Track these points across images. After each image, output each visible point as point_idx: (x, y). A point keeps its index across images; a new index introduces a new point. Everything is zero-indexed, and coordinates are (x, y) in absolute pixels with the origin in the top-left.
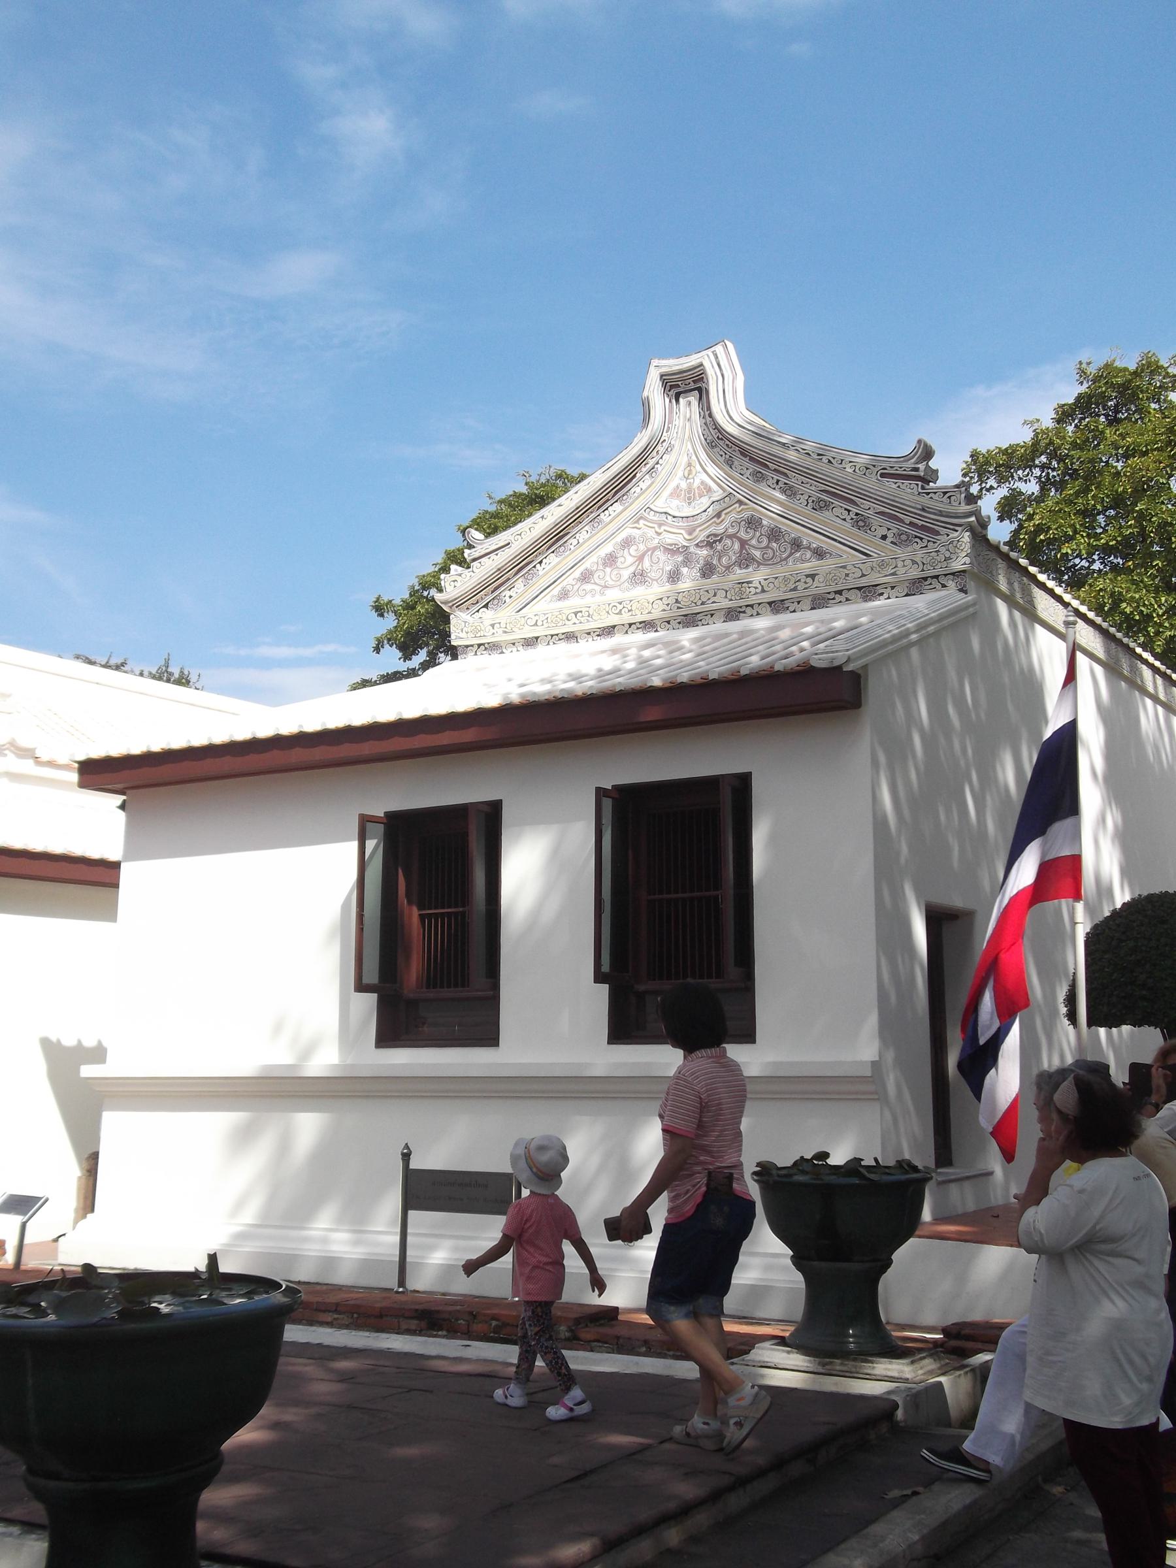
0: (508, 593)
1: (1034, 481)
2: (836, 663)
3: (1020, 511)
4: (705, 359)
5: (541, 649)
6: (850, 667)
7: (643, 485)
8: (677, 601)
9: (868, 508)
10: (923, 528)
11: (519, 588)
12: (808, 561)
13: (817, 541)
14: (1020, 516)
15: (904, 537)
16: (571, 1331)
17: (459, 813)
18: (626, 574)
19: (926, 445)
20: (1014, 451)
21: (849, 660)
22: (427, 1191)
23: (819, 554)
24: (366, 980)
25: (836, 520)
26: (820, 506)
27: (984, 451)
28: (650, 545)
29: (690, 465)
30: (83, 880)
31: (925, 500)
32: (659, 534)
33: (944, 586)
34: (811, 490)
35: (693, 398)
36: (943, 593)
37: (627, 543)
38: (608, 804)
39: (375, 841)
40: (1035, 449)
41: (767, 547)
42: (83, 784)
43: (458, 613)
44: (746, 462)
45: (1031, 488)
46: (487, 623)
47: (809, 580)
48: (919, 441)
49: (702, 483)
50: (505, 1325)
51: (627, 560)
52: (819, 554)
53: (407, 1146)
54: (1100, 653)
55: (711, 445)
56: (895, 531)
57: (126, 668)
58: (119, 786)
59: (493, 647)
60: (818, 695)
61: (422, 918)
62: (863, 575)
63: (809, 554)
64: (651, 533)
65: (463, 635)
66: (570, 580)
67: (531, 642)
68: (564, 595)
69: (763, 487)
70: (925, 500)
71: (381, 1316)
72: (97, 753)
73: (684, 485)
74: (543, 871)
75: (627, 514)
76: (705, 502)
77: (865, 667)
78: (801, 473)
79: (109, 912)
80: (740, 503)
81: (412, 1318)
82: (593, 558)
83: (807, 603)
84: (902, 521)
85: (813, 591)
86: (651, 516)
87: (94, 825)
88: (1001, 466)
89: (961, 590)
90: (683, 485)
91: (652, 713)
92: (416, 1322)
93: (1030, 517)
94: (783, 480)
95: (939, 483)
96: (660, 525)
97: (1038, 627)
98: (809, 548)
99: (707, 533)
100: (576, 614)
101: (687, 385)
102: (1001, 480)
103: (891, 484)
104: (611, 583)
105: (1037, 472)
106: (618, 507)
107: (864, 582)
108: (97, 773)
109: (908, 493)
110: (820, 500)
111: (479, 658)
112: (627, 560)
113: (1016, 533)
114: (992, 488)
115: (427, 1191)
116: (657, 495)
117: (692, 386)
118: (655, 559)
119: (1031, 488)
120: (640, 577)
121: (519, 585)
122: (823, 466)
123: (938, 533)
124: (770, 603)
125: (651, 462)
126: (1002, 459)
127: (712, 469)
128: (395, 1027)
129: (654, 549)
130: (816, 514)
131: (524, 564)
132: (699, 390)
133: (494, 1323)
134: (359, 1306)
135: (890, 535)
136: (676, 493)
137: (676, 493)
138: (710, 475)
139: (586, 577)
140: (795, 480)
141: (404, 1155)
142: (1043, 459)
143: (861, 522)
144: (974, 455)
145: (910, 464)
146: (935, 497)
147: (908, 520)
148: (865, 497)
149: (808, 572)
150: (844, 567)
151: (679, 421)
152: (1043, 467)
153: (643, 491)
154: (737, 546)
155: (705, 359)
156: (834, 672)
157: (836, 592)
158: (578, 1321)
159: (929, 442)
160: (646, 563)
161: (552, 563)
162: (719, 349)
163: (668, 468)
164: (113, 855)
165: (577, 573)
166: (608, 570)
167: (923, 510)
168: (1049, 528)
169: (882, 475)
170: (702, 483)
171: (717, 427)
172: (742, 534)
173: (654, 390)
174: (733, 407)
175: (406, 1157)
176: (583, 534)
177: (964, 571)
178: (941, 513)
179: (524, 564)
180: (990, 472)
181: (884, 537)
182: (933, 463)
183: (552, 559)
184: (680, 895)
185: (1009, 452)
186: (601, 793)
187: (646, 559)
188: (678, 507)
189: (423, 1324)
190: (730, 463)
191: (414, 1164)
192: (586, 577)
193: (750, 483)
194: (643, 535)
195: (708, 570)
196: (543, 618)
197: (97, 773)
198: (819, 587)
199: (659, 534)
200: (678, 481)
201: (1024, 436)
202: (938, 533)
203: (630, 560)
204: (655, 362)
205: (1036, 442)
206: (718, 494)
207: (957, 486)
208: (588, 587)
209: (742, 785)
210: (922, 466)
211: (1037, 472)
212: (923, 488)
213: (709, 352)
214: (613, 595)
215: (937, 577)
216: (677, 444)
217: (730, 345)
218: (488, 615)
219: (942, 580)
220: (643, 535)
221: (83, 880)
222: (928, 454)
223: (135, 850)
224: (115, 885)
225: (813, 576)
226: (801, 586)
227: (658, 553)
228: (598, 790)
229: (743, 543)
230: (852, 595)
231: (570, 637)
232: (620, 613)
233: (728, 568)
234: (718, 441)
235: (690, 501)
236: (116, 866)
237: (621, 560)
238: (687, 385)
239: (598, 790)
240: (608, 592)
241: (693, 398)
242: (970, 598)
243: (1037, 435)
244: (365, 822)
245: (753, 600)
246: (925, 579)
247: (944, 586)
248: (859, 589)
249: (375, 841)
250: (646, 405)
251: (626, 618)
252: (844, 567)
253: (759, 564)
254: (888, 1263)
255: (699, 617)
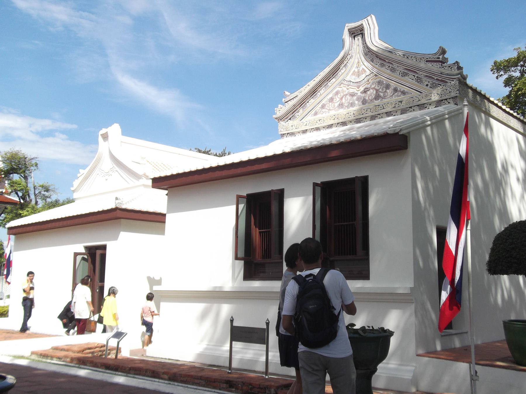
0: (297, 114)
1: (518, 72)
2: (396, 131)
3: (513, 83)
4: (364, 22)
5: (308, 134)
6: (401, 133)
7: (342, 71)
8: (354, 114)
9: (422, 74)
10: (441, 81)
11: (301, 112)
12: (400, 96)
13: (406, 89)
14: (513, 85)
15: (434, 85)
16: (276, 391)
17: (267, 194)
18: (337, 105)
19: (443, 48)
20: (510, 61)
21: (401, 130)
22: (239, 334)
23: (404, 93)
24: (239, 256)
25: (409, 80)
26: (404, 75)
27: (499, 61)
28: (345, 94)
29: (358, 62)
30: (154, 220)
31: (442, 70)
32: (348, 89)
33: (449, 103)
34: (401, 69)
35: (360, 37)
36: (449, 105)
37: (337, 93)
38: (318, 189)
39: (243, 205)
40: (518, 59)
41: (385, 92)
42: (153, 187)
43: (281, 122)
44: (378, 60)
45: (517, 74)
46: (290, 125)
47: (400, 103)
48: (440, 47)
49: (363, 69)
50: (254, 387)
51: (337, 99)
52: (404, 93)
53: (268, 320)
54: (522, 130)
55: (366, 54)
56: (431, 82)
57: (210, 153)
58: (166, 187)
59: (292, 134)
60: (389, 145)
61: (260, 232)
62: (419, 100)
63: (400, 93)
64: (345, 89)
65: (282, 130)
66: (318, 108)
67: (305, 132)
68: (316, 114)
69: (383, 69)
70: (442, 70)
71: (214, 382)
72: (157, 176)
73: (356, 70)
74: (298, 215)
75: (337, 82)
76: (364, 76)
77: (409, 133)
78: (397, 63)
79: (162, 231)
80: (376, 75)
81: (224, 383)
82: (326, 100)
83: (399, 112)
84: (433, 78)
85: (401, 107)
86: (345, 83)
87: (157, 201)
88: (505, 66)
89: (455, 104)
90: (358, 71)
91: (334, 154)
92: (225, 385)
93: (516, 85)
94: (391, 66)
95: (448, 63)
96: (348, 86)
97: (492, 121)
98: (400, 91)
99: (364, 87)
100: (319, 120)
101: (357, 32)
102: (505, 73)
103: (429, 65)
104: (332, 108)
105: (519, 68)
106: (334, 80)
107: (419, 103)
108: (159, 182)
109: (435, 68)
110: (404, 72)
111: (288, 138)
112: (337, 99)
113: (511, 91)
114: (502, 75)
115: (239, 334)
116: (347, 74)
117: (360, 33)
118: (346, 99)
119: (517, 74)
120: (341, 106)
121: (301, 111)
122: (405, 60)
123: (447, 82)
124: (386, 113)
125: (345, 62)
126: (506, 64)
127: (366, 63)
128: (249, 275)
129: (346, 95)
130: (403, 78)
131: (302, 103)
132: (362, 34)
133: (250, 387)
134: (208, 378)
135: (429, 84)
136: (354, 73)
137: (354, 73)
138: (367, 68)
139: (323, 107)
140: (395, 65)
141: (266, 323)
142: (522, 63)
143: (419, 80)
144: (495, 63)
145: (437, 56)
146: (446, 68)
147: (436, 78)
148: (420, 70)
149: (399, 100)
150: (412, 98)
151: (355, 47)
152: (522, 66)
153: (342, 74)
154: (375, 92)
155: (364, 22)
156: (396, 135)
157: (410, 107)
158: (278, 387)
159: (444, 47)
160: (344, 100)
161: (312, 102)
162: (369, 18)
163: (351, 64)
164: (164, 211)
165: (320, 106)
166: (331, 103)
167: (441, 74)
168: (523, 89)
169: (426, 61)
170: (363, 69)
171: (368, 48)
172: (377, 88)
173: (346, 36)
174: (375, 40)
175: (232, 321)
176: (322, 91)
177: (456, 97)
178: (448, 74)
179: (302, 103)
180: (501, 69)
181: (427, 85)
182: (446, 56)
183: (312, 101)
184: (346, 223)
185: (508, 61)
186: (315, 185)
187: (344, 99)
188: (354, 79)
189: (228, 385)
190: (372, 61)
191: (235, 324)
192: (323, 107)
193: (380, 68)
194: (343, 90)
195: (364, 102)
196: (308, 122)
197: (159, 182)
198: (403, 105)
199: (348, 89)
200: (354, 69)
201: (515, 55)
202: (447, 82)
203: (338, 99)
204: (347, 25)
205: (518, 57)
206: (368, 72)
207: (454, 64)
208: (324, 110)
209: (365, 180)
210: (441, 57)
211: (519, 68)
212: (441, 65)
213: (365, 19)
214: (332, 113)
215: (446, 99)
216: (354, 55)
217: (373, 17)
218: (290, 122)
219: (448, 100)
220: (343, 90)
221: (154, 220)
222: (444, 52)
223: (171, 208)
224: (164, 222)
225: (401, 102)
226: (397, 106)
227: (348, 96)
228: (314, 183)
229: (377, 91)
230: (415, 108)
231: (318, 129)
232: (334, 119)
233: (371, 100)
234: (370, 54)
235: (358, 76)
236: (164, 215)
237: (335, 99)
238: (357, 32)
239: (314, 183)
240: (330, 112)
241: (360, 37)
242: (459, 107)
243: (519, 54)
244: (239, 197)
245: (380, 112)
246: (442, 100)
247: (449, 103)
248: (418, 106)
249: (243, 205)
250: (343, 41)
251: (337, 121)
252: (412, 98)
253: (382, 98)
254: (375, 370)
255: (361, 119)
